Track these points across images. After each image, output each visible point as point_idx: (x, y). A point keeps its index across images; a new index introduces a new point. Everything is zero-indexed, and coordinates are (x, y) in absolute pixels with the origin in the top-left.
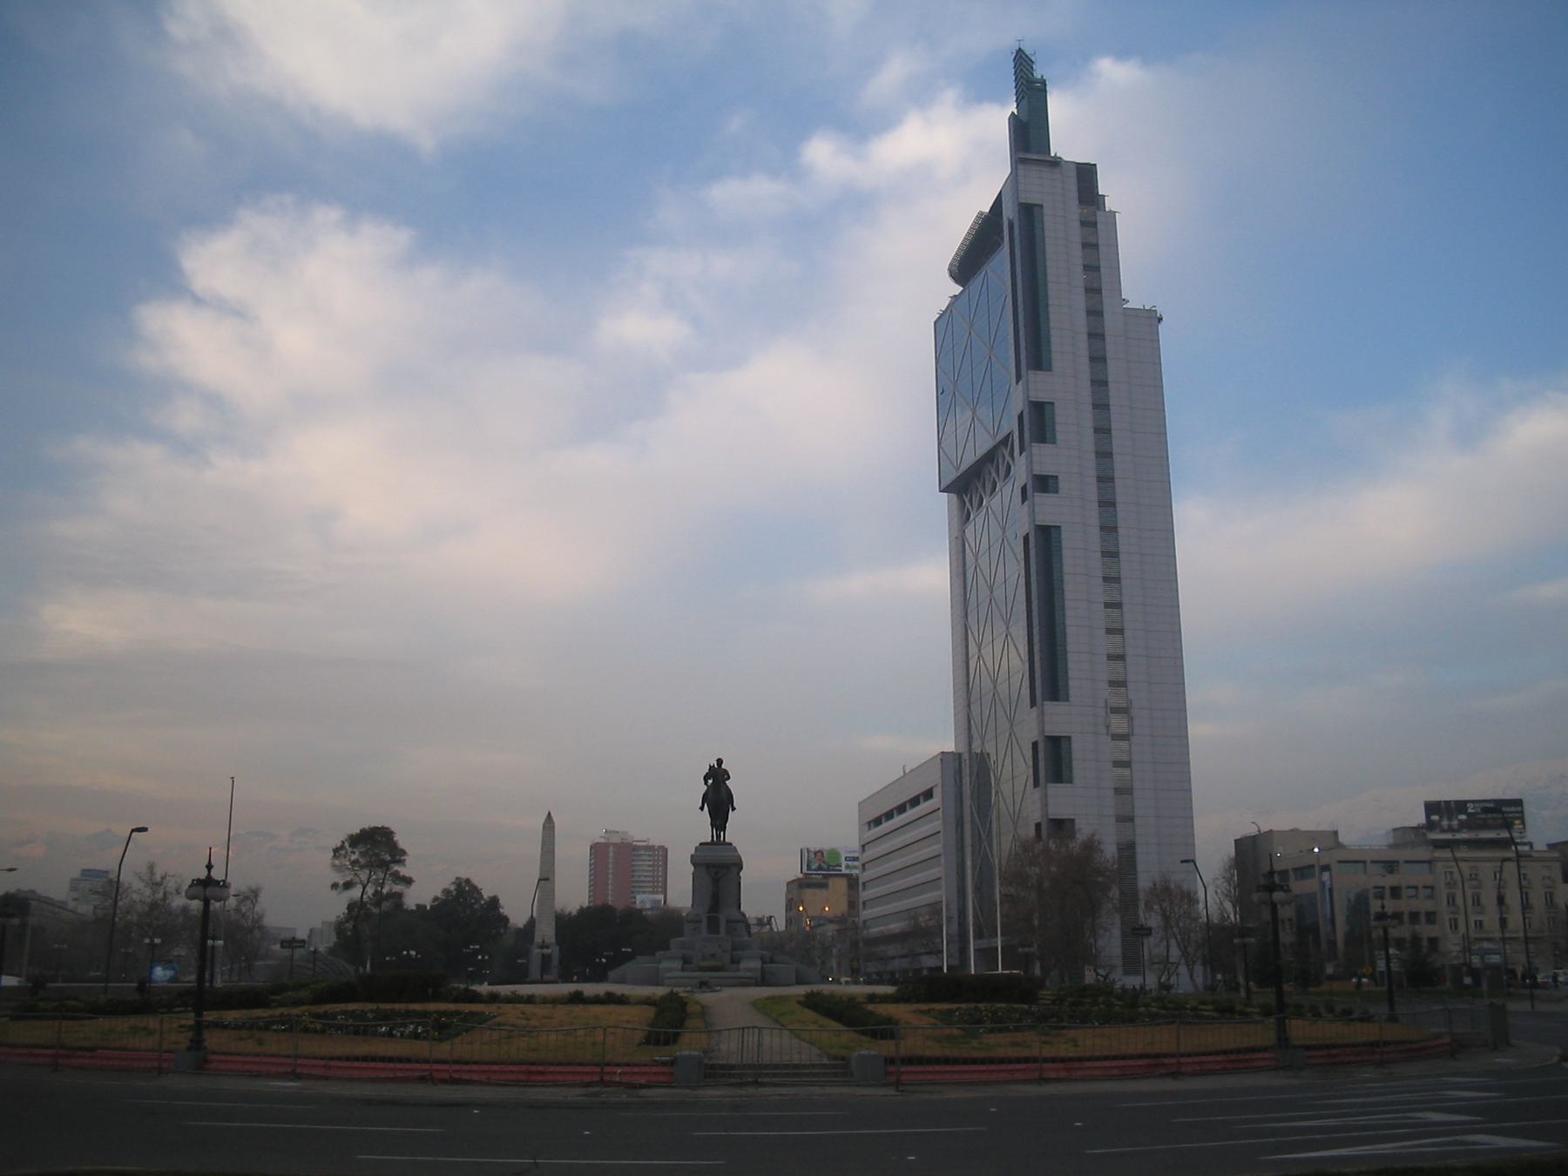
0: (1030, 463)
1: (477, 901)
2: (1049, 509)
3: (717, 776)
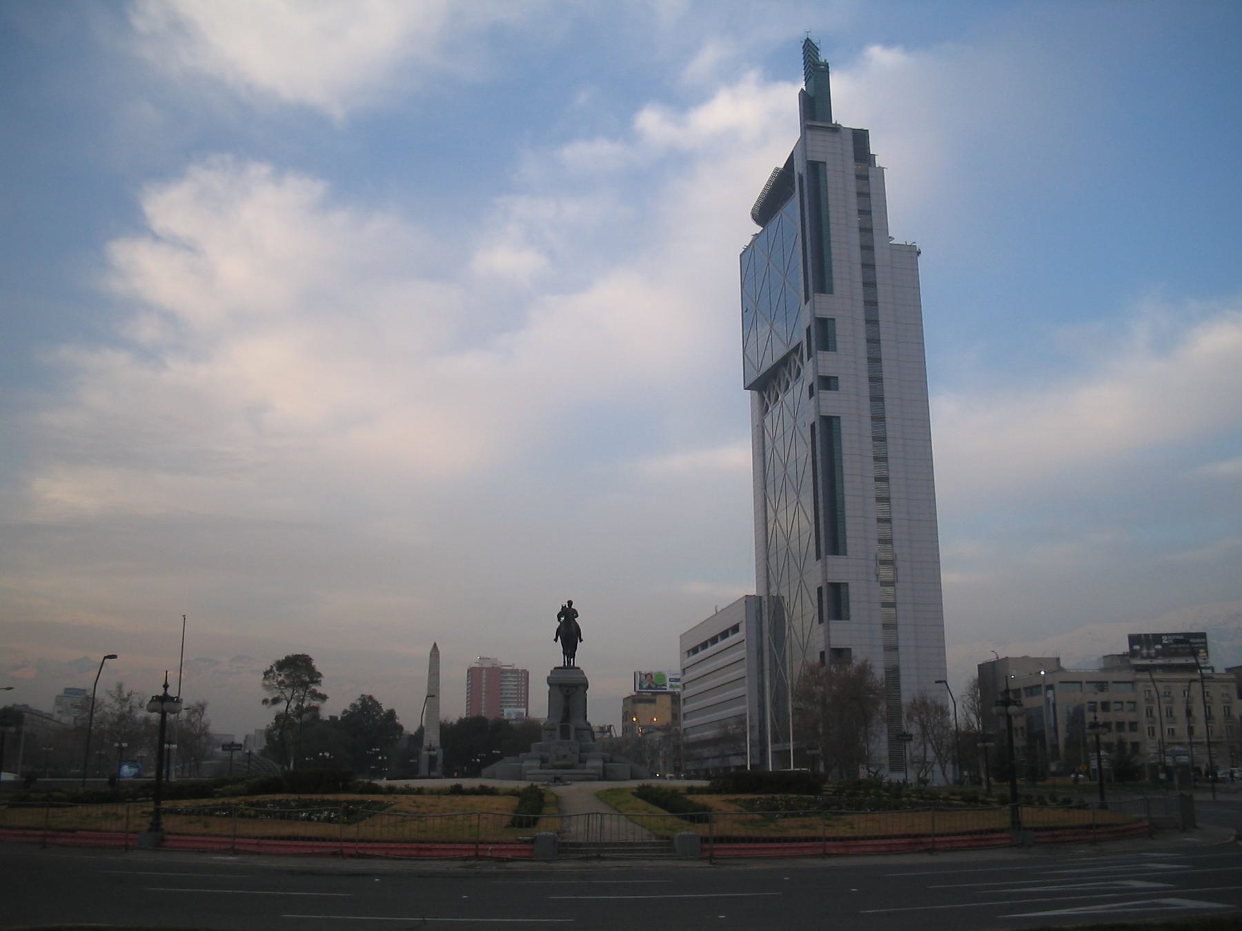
0: (816, 366)
1: (378, 713)
2: (831, 403)
3: (568, 614)
